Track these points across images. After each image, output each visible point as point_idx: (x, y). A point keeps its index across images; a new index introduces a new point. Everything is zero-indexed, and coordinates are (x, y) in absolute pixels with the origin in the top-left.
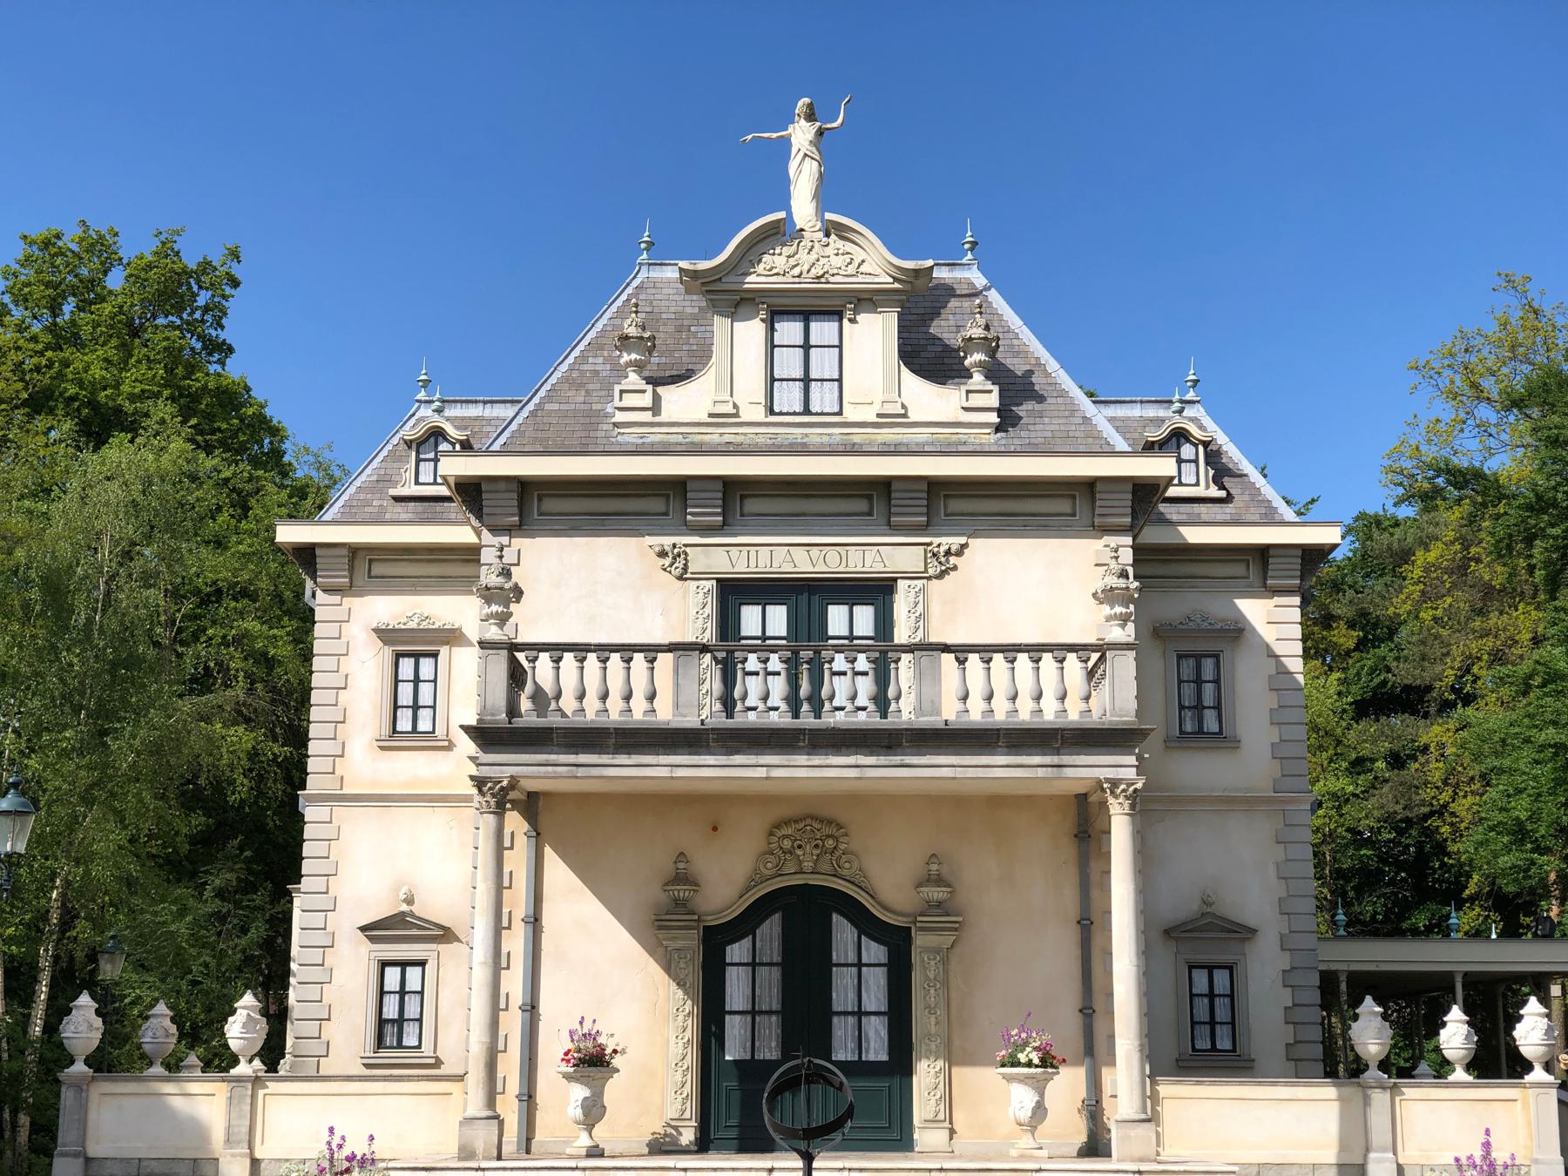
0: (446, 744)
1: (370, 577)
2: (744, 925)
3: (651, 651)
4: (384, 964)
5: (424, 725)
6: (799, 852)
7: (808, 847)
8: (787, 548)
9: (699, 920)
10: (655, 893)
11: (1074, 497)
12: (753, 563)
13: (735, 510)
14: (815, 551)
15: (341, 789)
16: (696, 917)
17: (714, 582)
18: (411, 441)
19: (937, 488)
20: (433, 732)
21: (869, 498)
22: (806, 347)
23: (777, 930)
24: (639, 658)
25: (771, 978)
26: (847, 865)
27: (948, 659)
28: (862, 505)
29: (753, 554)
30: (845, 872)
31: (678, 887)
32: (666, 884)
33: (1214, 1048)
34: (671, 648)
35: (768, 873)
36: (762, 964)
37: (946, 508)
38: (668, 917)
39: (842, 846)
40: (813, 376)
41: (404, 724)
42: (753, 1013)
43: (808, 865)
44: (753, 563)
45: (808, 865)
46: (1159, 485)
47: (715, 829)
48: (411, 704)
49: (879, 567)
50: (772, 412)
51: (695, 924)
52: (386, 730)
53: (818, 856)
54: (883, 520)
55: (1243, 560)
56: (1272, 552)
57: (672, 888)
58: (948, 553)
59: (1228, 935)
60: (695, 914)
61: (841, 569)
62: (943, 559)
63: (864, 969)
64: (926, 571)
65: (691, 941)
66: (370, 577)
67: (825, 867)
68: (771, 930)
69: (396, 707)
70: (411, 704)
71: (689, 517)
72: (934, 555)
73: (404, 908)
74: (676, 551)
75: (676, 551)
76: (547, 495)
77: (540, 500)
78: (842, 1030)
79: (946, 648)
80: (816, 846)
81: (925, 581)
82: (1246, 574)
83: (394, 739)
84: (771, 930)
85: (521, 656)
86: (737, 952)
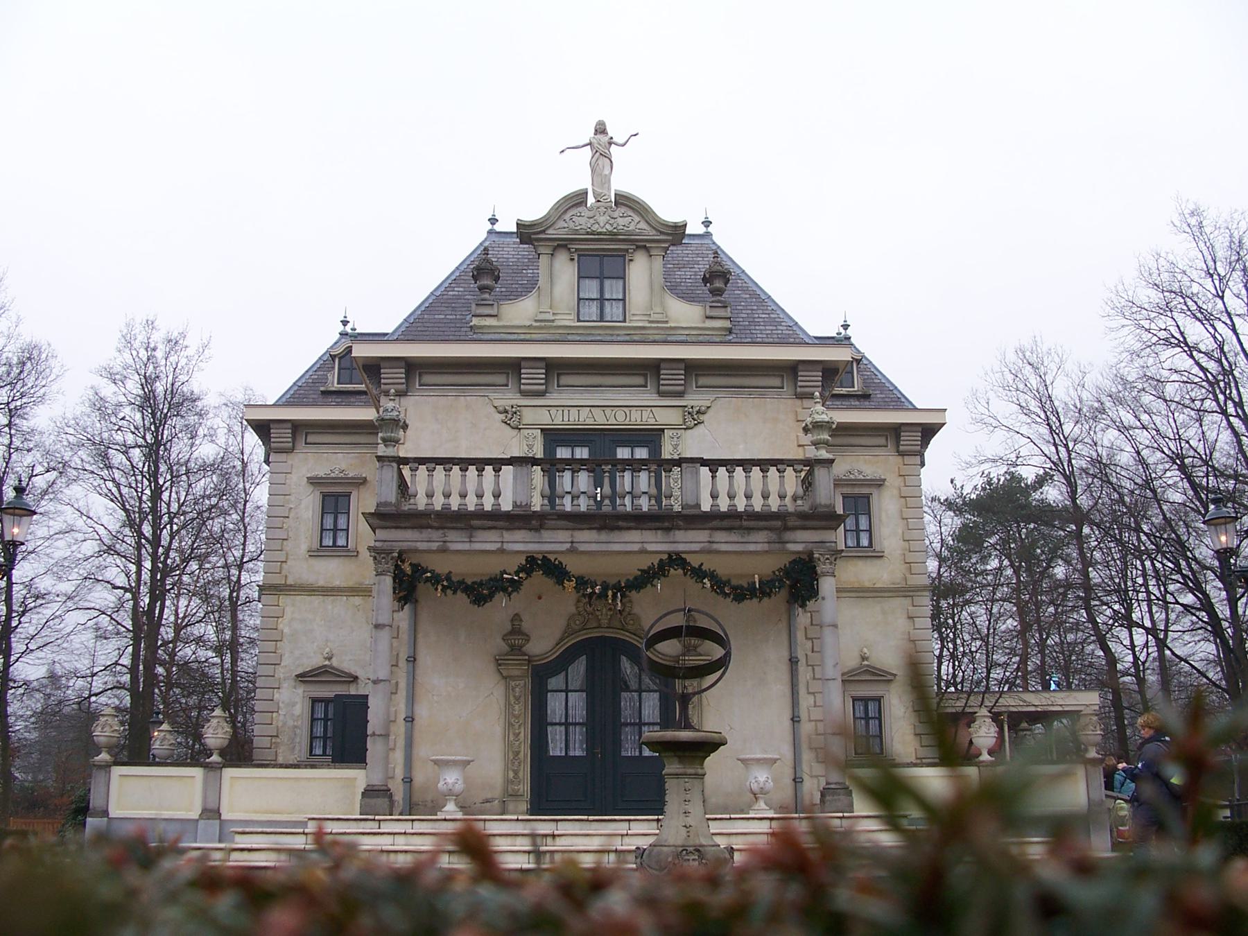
0: (355, 554)
1: (306, 444)
2: (561, 663)
3: (498, 464)
4: (314, 701)
5: (341, 542)
6: (598, 613)
7: (604, 610)
8: (589, 409)
9: (529, 661)
10: (500, 645)
11: (782, 376)
12: (566, 419)
13: (554, 382)
14: (608, 411)
15: (379, 828)
16: (527, 657)
17: (539, 431)
18: (335, 356)
19: (694, 369)
20: (347, 547)
21: (645, 376)
22: (602, 300)
23: (584, 662)
24: (489, 469)
25: (578, 702)
26: (631, 622)
27: (705, 471)
28: (639, 380)
29: (566, 412)
30: (629, 627)
31: (515, 637)
32: (505, 635)
33: (858, 545)
34: (511, 461)
35: (577, 627)
36: (560, 724)
37: (696, 383)
38: (506, 658)
39: (627, 609)
40: (607, 296)
41: (328, 541)
42: (567, 724)
43: (605, 622)
44: (566, 419)
45: (605, 622)
46: (838, 370)
47: (540, 598)
48: (332, 527)
49: (652, 421)
50: (579, 320)
51: (526, 662)
52: (316, 545)
53: (611, 616)
54: (654, 390)
55: (883, 435)
56: (903, 428)
57: (511, 637)
58: (698, 412)
59: (876, 678)
60: (526, 655)
61: (626, 422)
62: (695, 416)
63: (564, 688)
64: (685, 423)
65: (523, 686)
66: (306, 444)
67: (617, 624)
68: (579, 668)
69: (322, 530)
70: (332, 527)
71: (522, 386)
72: (689, 413)
73: (327, 663)
74: (514, 410)
75: (514, 410)
76: (426, 373)
77: (420, 375)
78: (628, 735)
79: (704, 462)
80: (610, 609)
81: (683, 431)
82: (885, 444)
83: (320, 551)
84: (579, 668)
85: (406, 471)
86: (555, 682)
